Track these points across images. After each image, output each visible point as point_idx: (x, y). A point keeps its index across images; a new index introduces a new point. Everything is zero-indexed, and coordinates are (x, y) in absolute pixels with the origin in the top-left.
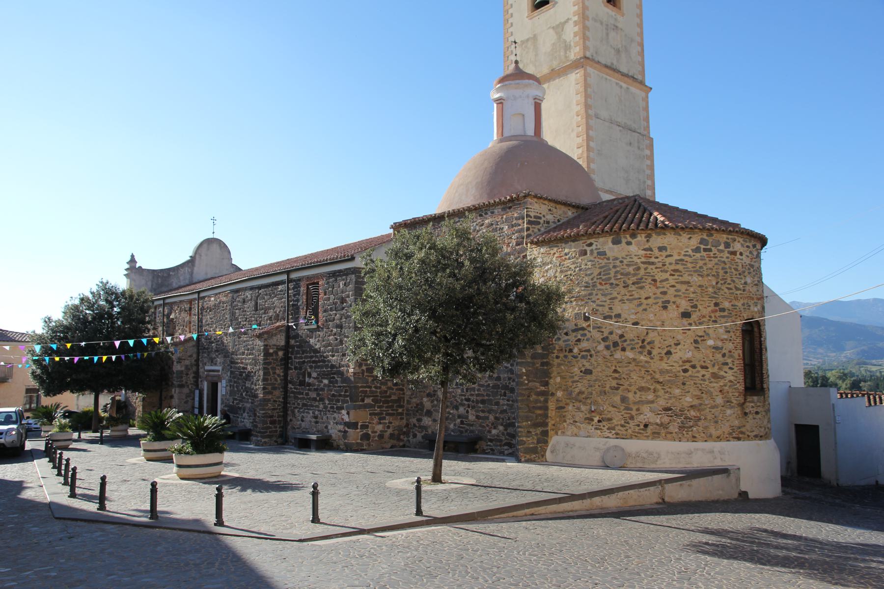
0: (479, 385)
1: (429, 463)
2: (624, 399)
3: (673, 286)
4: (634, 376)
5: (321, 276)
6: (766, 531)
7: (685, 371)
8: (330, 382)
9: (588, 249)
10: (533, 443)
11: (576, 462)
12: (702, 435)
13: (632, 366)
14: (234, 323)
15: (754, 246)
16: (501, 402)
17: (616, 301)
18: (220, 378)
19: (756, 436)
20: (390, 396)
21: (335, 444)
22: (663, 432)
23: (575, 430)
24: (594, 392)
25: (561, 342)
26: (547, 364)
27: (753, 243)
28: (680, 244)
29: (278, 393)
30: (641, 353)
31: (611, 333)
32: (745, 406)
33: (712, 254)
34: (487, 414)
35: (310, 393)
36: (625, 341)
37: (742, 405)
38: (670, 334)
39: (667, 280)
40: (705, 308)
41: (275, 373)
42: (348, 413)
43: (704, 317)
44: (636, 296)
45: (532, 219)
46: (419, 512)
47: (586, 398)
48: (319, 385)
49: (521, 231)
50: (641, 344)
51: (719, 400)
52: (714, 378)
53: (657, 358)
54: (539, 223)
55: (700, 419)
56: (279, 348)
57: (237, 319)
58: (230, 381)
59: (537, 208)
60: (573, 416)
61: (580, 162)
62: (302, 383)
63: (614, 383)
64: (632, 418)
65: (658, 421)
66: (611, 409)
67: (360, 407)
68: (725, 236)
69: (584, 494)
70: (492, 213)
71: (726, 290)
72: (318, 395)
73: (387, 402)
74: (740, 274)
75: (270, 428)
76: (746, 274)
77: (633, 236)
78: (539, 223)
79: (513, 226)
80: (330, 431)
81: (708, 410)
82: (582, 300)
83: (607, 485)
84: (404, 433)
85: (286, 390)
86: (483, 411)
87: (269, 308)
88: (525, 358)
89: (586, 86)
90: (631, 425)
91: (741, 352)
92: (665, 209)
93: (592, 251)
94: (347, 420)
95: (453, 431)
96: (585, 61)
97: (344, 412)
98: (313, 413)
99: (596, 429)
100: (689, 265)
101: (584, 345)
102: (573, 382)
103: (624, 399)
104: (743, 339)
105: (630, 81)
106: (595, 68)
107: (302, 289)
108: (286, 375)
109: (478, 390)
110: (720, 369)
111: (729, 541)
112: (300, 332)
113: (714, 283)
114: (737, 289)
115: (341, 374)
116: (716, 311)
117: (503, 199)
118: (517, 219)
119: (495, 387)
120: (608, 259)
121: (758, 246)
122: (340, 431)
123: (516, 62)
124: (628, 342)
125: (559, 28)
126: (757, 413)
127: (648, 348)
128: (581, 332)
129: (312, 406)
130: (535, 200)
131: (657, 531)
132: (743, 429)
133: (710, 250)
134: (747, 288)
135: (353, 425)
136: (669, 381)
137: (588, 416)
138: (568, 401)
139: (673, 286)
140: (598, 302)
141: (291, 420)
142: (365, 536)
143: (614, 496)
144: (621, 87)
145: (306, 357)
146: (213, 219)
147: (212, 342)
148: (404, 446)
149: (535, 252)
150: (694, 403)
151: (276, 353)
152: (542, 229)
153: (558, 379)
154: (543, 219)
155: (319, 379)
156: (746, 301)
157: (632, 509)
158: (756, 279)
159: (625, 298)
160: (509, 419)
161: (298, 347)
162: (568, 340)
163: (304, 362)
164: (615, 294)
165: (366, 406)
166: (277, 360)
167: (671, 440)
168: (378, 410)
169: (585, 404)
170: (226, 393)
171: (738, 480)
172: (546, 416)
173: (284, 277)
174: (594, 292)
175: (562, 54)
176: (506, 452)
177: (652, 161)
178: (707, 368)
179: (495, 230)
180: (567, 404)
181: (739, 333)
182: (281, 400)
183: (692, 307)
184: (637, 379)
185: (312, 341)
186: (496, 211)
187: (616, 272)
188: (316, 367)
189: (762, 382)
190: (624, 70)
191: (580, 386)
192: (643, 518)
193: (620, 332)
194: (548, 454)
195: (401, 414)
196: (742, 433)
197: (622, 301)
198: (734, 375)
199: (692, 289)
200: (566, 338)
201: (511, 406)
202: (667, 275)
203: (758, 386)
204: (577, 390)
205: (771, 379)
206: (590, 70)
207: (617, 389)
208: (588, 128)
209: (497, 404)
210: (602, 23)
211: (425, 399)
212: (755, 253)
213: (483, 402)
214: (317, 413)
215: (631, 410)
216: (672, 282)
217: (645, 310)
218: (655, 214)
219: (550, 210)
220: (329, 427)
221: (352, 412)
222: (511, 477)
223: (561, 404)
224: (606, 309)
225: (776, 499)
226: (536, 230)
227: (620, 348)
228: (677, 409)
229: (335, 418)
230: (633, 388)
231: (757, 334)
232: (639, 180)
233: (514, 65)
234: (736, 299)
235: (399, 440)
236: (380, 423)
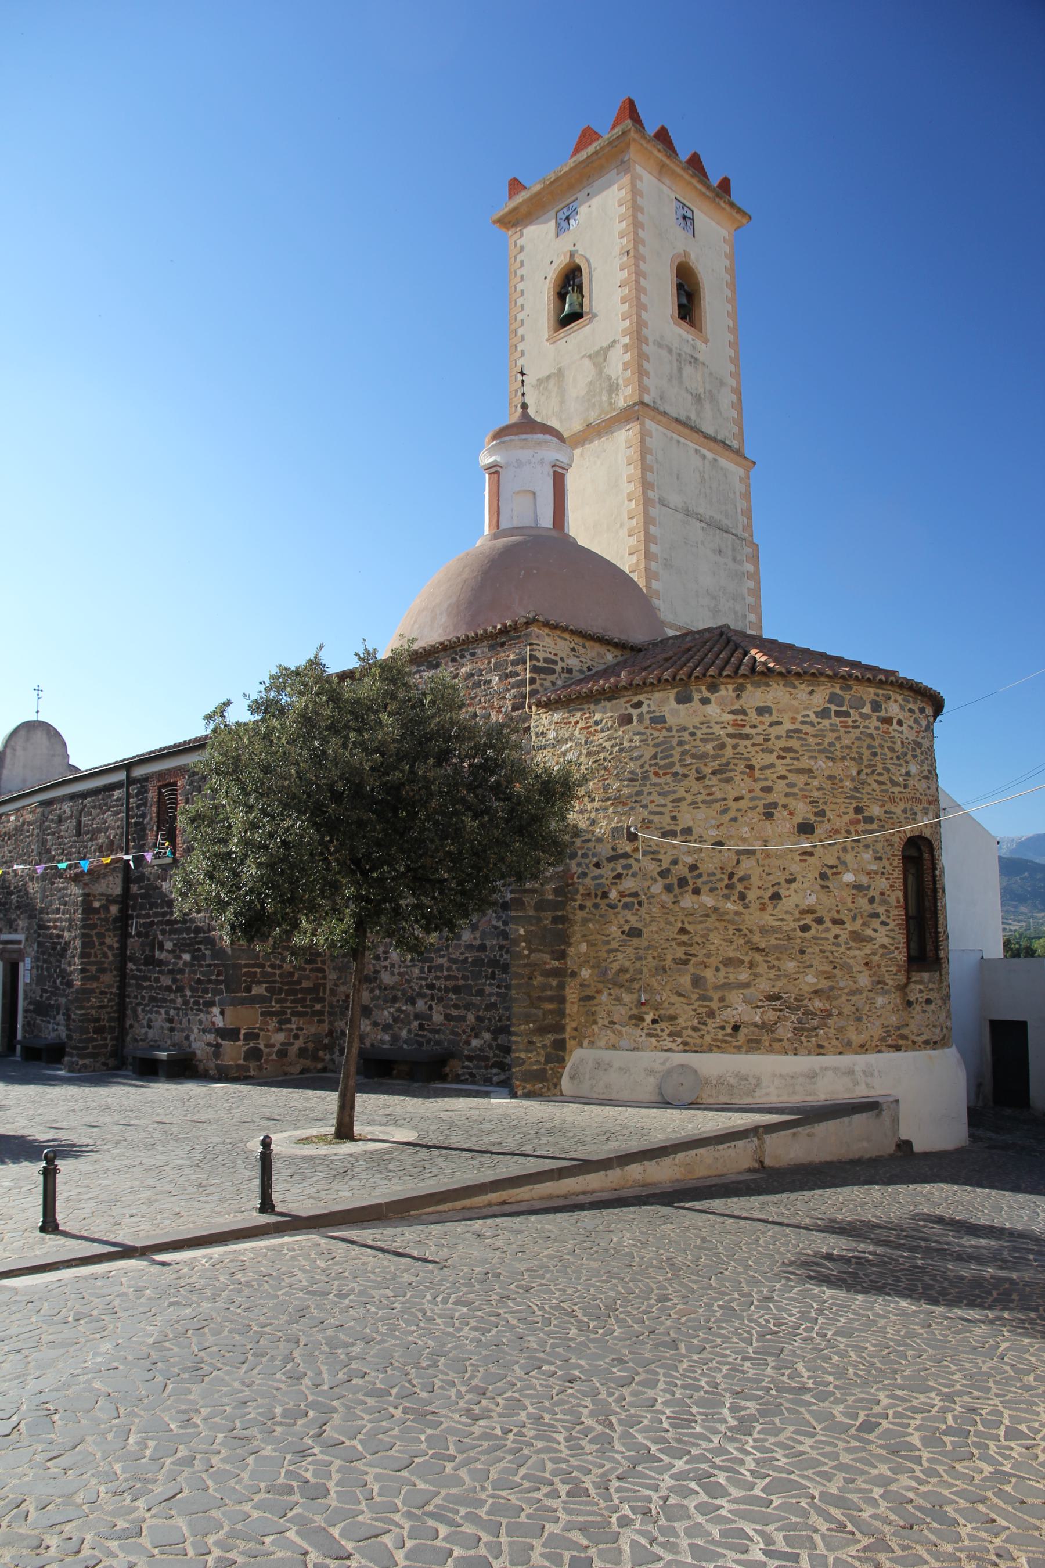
0: (451, 960)
1: (330, 1100)
2: (697, 981)
3: (783, 777)
4: (716, 939)
6: (940, 1220)
7: (805, 928)
8: (193, 958)
9: (635, 713)
10: (538, 1062)
11: (614, 1096)
12: (834, 1042)
13: (710, 922)
14: (45, 857)
15: (922, 710)
16: (488, 989)
17: (684, 806)
18: (21, 955)
19: (926, 1043)
20: (299, 982)
21: (201, 1067)
22: (766, 1038)
24: (645, 969)
25: (588, 881)
26: (563, 920)
27: (920, 704)
28: (795, 703)
29: (109, 978)
30: (727, 897)
31: (675, 862)
32: (907, 990)
33: (849, 720)
34: (463, 1012)
35: (162, 978)
36: (700, 876)
37: (903, 988)
38: (779, 862)
39: (772, 766)
40: (840, 815)
41: (102, 944)
42: (222, 1013)
43: (837, 832)
44: (719, 795)
45: (541, 664)
46: (266, 1205)
47: (632, 980)
48: (175, 964)
49: (522, 683)
50: (726, 881)
51: (864, 980)
52: (854, 940)
53: (755, 906)
54: (553, 672)
55: (831, 1015)
56: (111, 900)
57: (49, 851)
58: (37, 959)
59: (548, 645)
61: (635, 577)
62: (151, 961)
63: (680, 953)
64: (711, 1014)
65: (757, 1019)
66: (674, 999)
67: (242, 1002)
68: (872, 690)
69: (611, 1159)
70: (473, 654)
71: (875, 786)
72: (174, 981)
73: (293, 992)
74: (898, 758)
75: (96, 1040)
76: (909, 757)
77: (713, 688)
78: (553, 672)
79: (507, 676)
80: (194, 1045)
81: (844, 998)
82: (625, 804)
83: (658, 1138)
84: (325, 1047)
85: (123, 974)
86: (456, 1007)
87: (99, 830)
88: (524, 909)
89: (644, 451)
90: (709, 1028)
91: (900, 894)
92: (770, 646)
93: (641, 716)
94: (221, 1025)
95: (406, 1042)
96: (640, 410)
97: (216, 1010)
98: (167, 1013)
99: (649, 1035)
100: (811, 740)
101: (629, 884)
102: (609, 951)
103: (697, 981)
104: (905, 872)
105: (719, 448)
106: (659, 423)
107: (150, 794)
108: (123, 947)
109: (449, 969)
110: (864, 924)
111: (871, 1248)
112: (147, 871)
113: (854, 773)
114: (894, 783)
115: (211, 942)
116: (858, 822)
117: (490, 629)
118: (514, 663)
119: (477, 962)
120: (670, 730)
121: (929, 711)
122: (209, 1044)
123: (524, 406)
124: (705, 878)
125: (599, 357)
126: (928, 1001)
127: (740, 887)
128: (623, 861)
129: (165, 1000)
130: (547, 630)
131: (738, 1230)
132: (905, 1031)
133: (847, 714)
134: (911, 782)
135: (231, 1034)
136: (776, 947)
137: (635, 1012)
138: (600, 986)
139: (783, 777)
140: (652, 807)
141: (131, 1026)
142: (132, 1263)
143: (667, 1161)
144: (704, 457)
145: (156, 915)
146: (38, 689)
147: (12, 893)
148: (325, 1070)
149: (545, 721)
150: (819, 987)
151: (105, 908)
152: (560, 683)
153: (584, 947)
154: (561, 664)
155: (175, 952)
156: (908, 806)
157: (701, 1183)
158: (926, 768)
159: (700, 798)
160: (500, 1020)
161: (143, 896)
162: (601, 876)
163: (152, 923)
164: (681, 793)
165: (254, 1000)
166: (106, 920)
167: (779, 1053)
168: (276, 1007)
169: (629, 990)
170: (32, 979)
171: (895, 1120)
172: (562, 1013)
173: (122, 776)
174: (646, 790)
175: (605, 398)
176: (495, 1079)
177: (758, 582)
178: (843, 923)
179: (477, 685)
180: (599, 992)
181: (897, 861)
182: (114, 990)
183: (816, 814)
184: (719, 943)
185: (165, 886)
186: (479, 651)
187: (684, 753)
188: (171, 932)
189: (937, 948)
190: (710, 430)
191: (622, 959)
192: (717, 1204)
193: (689, 860)
194: (566, 1084)
195: (320, 1013)
196: (904, 1037)
197: (694, 804)
198: (888, 935)
199: (816, 783)
200: (597, 872)
201: (504, 997)
202: (772, 758)
203: (931, 954)
204: (616, 966)
205: (953, 944)
206: (649, 424)
207: (686, 962)
208: (648, 520)
209: (480, 993)
210: (670, 351)
212: (924, 723)
213: (456, 990)
214: (172, 1012)
215: (711, 1000)
216: (781, 770)
217: (735, 819)
218: (753, 652)
219: (573, 649)
220: (192, 1038)
221: (229, 1011)
222: (487, 1126)
223: (589, 992)
224: (666, 819)
225: (959, 1151)
226: (547, 684)
227: (690, 888)
228: (790, 997)
229: (200, 1022)
230: (713, 961)
231: (927, 864)
232: (736, 613)
233: (519, 410)
234: (892, 800)
235: (316, 1058)
236: (281, 1030)
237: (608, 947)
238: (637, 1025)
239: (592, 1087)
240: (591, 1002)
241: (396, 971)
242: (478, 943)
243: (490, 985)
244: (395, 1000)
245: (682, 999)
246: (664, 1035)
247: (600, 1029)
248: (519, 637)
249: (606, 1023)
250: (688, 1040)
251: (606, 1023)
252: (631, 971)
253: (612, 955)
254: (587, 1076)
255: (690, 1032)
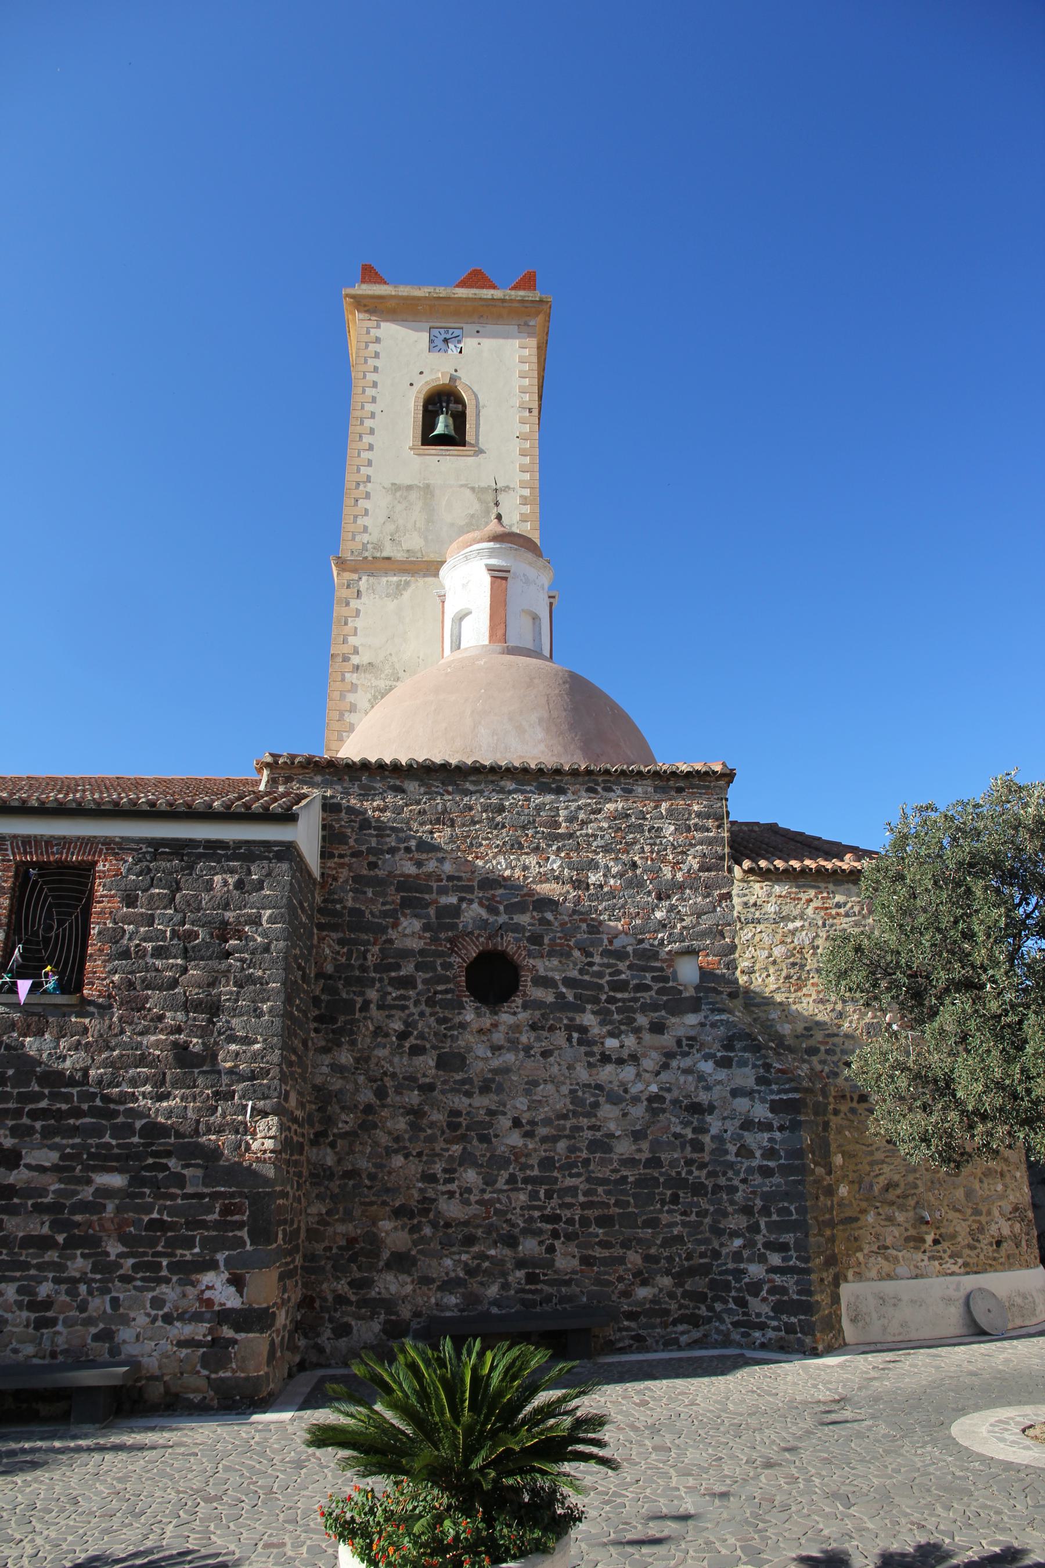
5: (114, 847)
8: (136, 1180)
11: (914, 1336)
16: (665, 1219)
23: (887, 1267)
47: (905, 1197)
60: (877, 1237)
66: (952, 1215)
86: (605, 1245)
95: (495, 1303)
102: (871, 1164)
137: (912, 1232)
138: (864, 1204)
160: (689, 1258)
169: (902, 1208)
176: (684, 1339)
180: (864, 1211)
204: (882, 1181)
209: (653, 1223)
211: (386, 1225)
229: (158, 1303)
237: (869, 1159)
238: (916, 1248)
239: (884, 1328)
240: (854, 1225)
241: (473, 1198)
242: (646, 1155)
243: (669, 1212)
244: (469, 1241)
245: (958, 1215)
246: (945, 1256)
247: (867, 1256)
248: (708, 787)
249: (875, 1248)
250: (968, 1260)
251: (875, 1248)
252: (902, 1185)
253: (876, 1168)
254: (875, 1316)
255: (967, 1251)
